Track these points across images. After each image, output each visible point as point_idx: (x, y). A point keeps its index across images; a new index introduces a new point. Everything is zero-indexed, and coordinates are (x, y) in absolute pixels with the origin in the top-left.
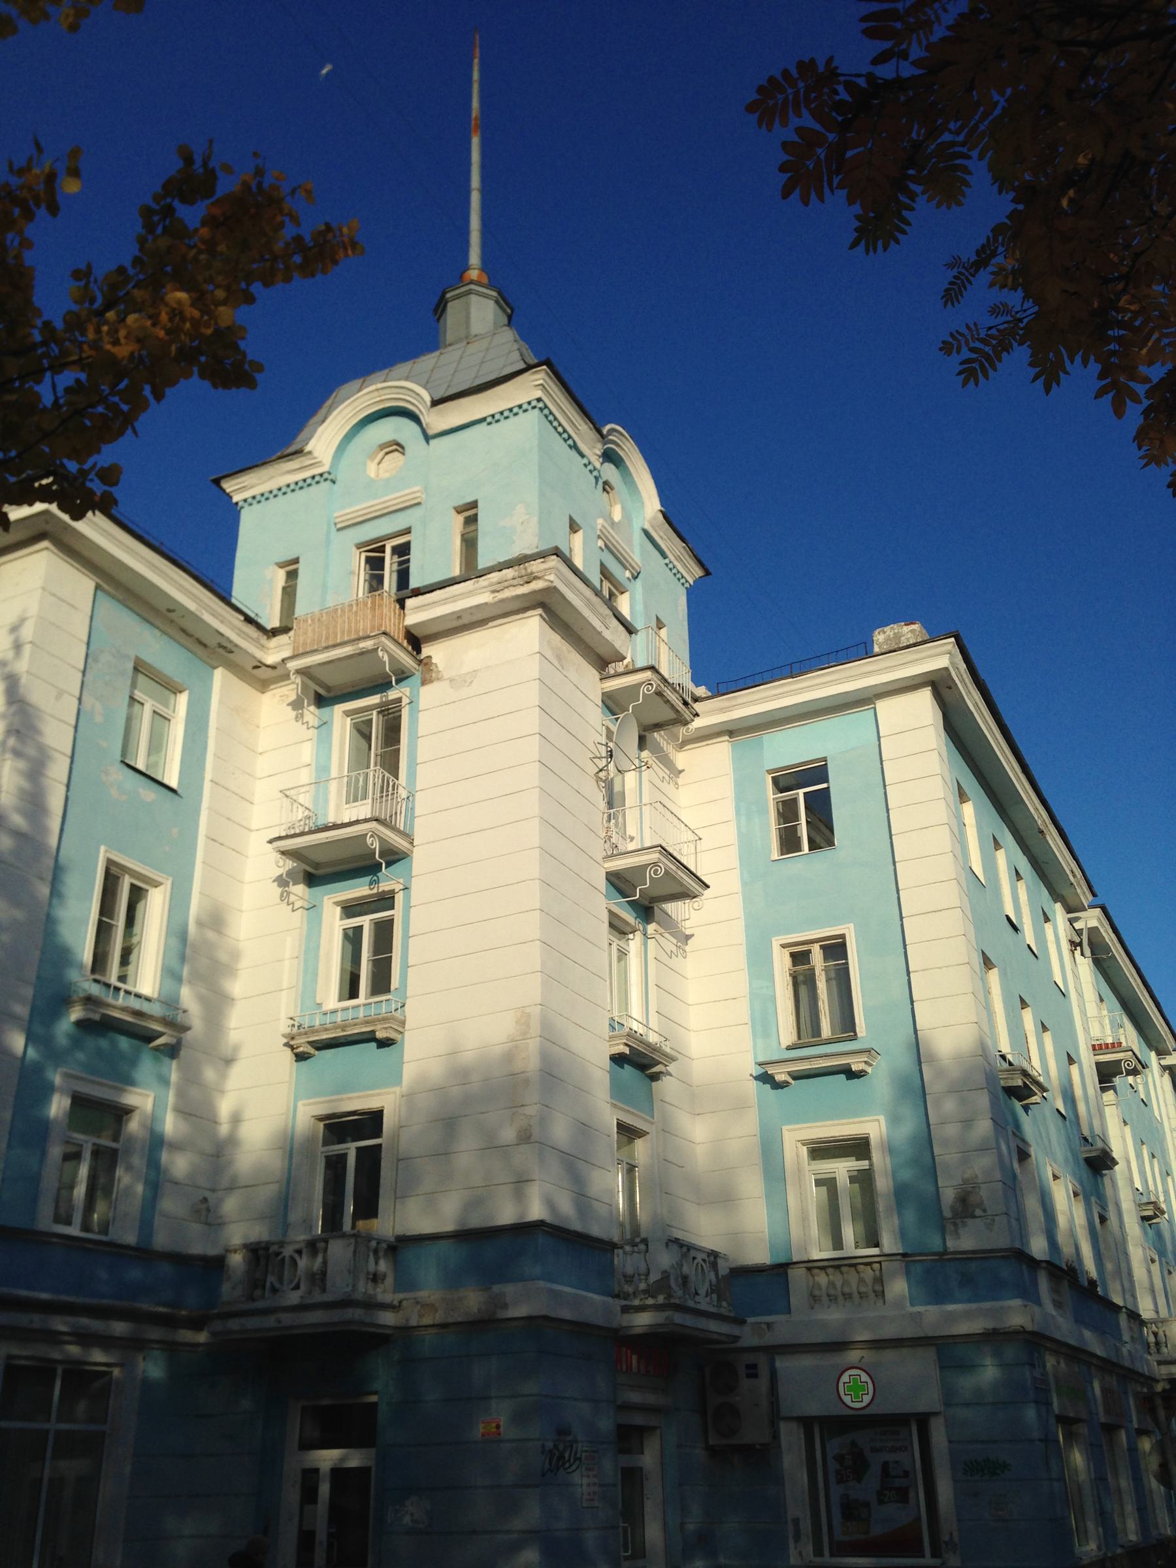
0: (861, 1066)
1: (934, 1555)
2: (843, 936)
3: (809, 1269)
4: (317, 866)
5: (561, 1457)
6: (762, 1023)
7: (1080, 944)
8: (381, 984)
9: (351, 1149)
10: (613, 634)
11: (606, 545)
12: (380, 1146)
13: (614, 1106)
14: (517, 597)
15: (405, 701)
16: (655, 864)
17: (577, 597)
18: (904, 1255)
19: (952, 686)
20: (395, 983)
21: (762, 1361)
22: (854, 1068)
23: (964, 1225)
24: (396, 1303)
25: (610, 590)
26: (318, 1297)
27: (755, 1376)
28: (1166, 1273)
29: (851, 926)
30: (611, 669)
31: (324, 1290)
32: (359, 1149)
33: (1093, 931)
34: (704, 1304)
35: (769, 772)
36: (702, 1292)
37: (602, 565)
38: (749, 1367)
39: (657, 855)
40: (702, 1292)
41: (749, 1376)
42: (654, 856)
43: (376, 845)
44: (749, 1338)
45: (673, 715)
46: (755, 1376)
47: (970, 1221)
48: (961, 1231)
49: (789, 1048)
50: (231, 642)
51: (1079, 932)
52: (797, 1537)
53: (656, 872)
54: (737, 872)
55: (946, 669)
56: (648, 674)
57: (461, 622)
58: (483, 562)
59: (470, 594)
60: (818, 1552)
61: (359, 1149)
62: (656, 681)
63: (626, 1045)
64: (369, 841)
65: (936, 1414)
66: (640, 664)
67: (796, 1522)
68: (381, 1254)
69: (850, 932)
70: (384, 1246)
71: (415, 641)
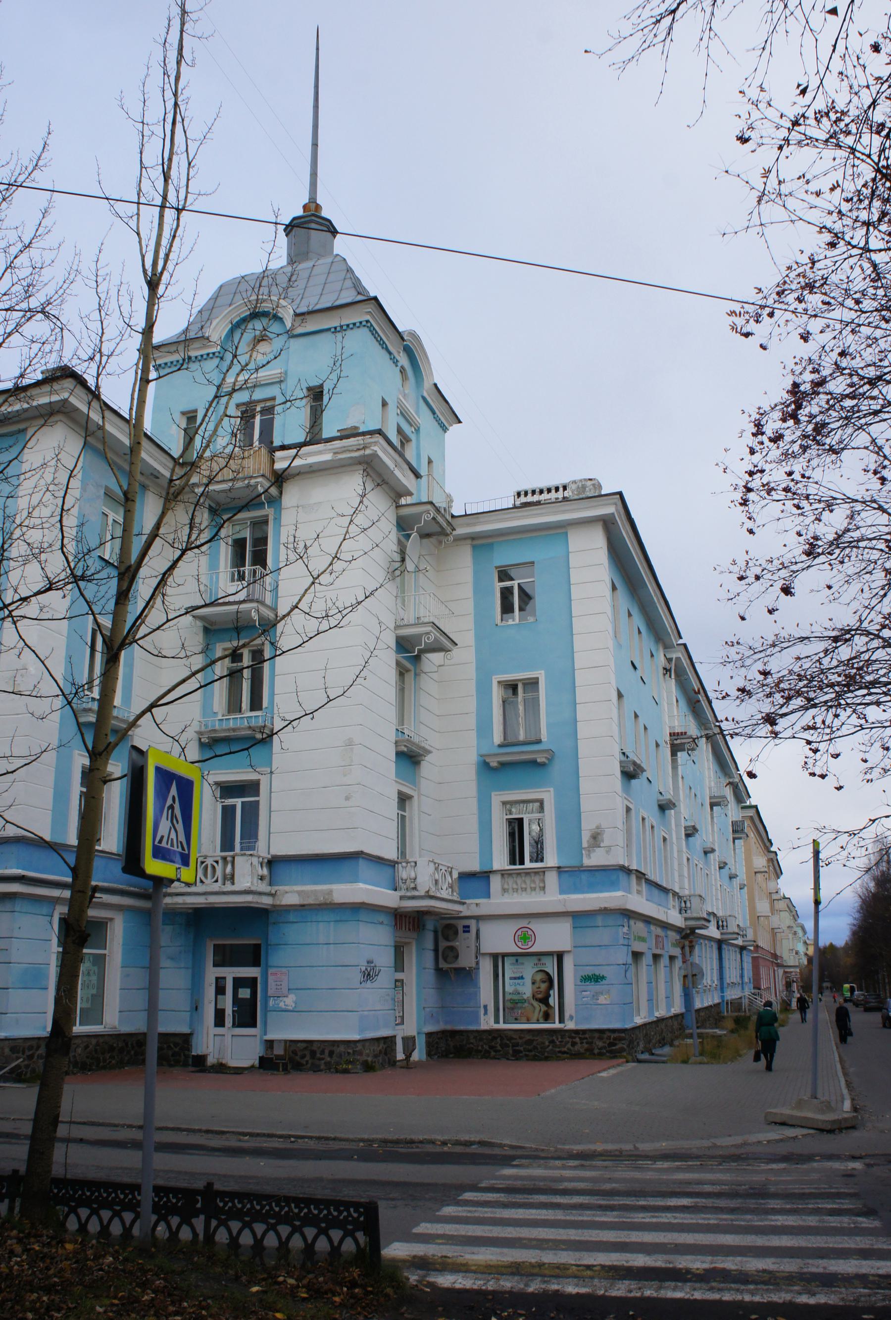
0: (544, 760)
1: (560, 1022)
2: (537, 678)
3: (503, 875)
4: (212, 623)
5: (369, 974)
6: (484, 728)
7: (670, 670)
8: (256, 703)
9: (238, 802)
10: (406, 479)
11: (401, 412)
12: (258, 802)
13: (396, 782)
14: (351, 458)
15: (271, 518)
16: (428, 633)
17: (387, 458)
18: (559, 868)
19: (614, 523)
20: (265, 703)
21: (473, 924)
22: (539, 760)
23: (594, 851)
24: (273, 892)
25: (400, 431)
26: (229, 887)
27: (469, 932)
28: (737, 307)
29: (543, 672)
30: (403, 501)
31: (233, 883)
32: (242, 802)
33: (678, 659)
34: (444, 894)
35: (496, 568)
36: (444, 888)
37: (398, 425)
38: (465, 927)
39: (430, 628)
40: (444, 888)
41: (464, 932)
42: (429, 629)
43: (256, 617)
44: (465, 911)
45: (439, 529)
46: (469, 932)
47: (597, 850)
48: (592, 855)
49: (500, 746)
50: (158, 471)
51: (669, 660)
52: (486, 1013)
53: (428, 638)
54: (473, 632)
55: (613, 514)
56: (429, 507)
57: (311, 469)
58: (328, 431)
59: (320, 453)
60: (497, 1021)
61: (242, 802)
62: (433, 513)
63: (405, 746)
64: (253, 614)
65: (569, 952)
66: (425, 500)
67: (485, 1007)
68: (264, 865)
69: (541, 675)
70: (266, 860)
71: (280, 479)
